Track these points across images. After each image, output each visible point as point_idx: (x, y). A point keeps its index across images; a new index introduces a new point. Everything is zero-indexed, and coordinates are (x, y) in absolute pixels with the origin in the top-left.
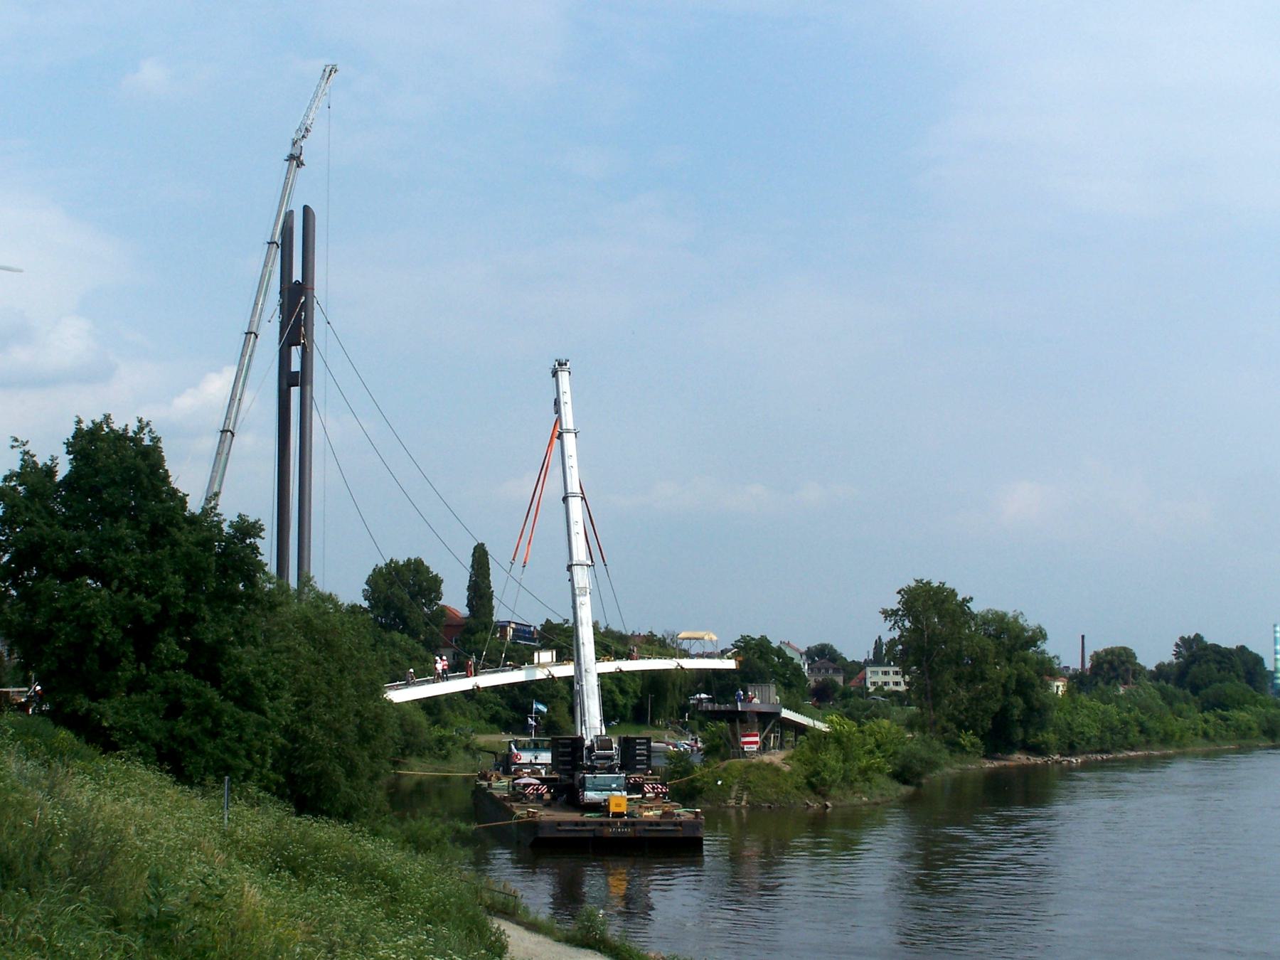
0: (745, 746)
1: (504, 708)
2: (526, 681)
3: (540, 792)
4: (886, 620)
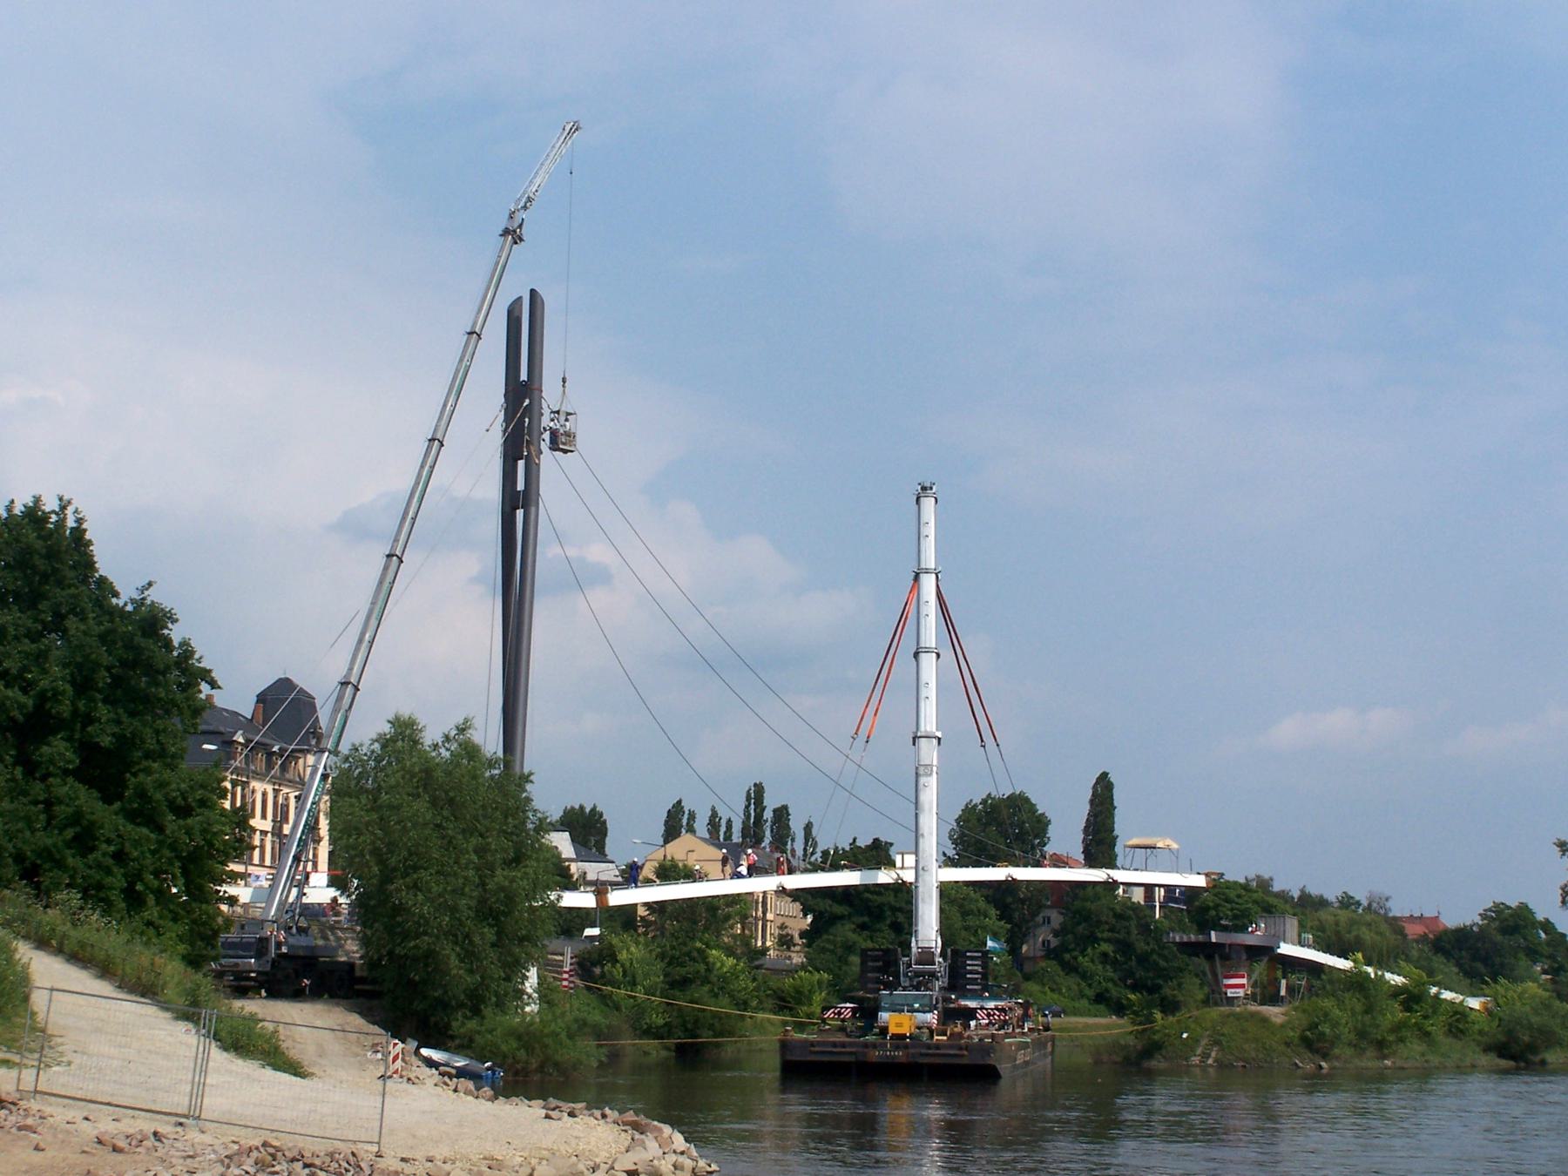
0: (1229, 991)
1: (1115, 984)
2: (860, 885)
3: (842, 1016)
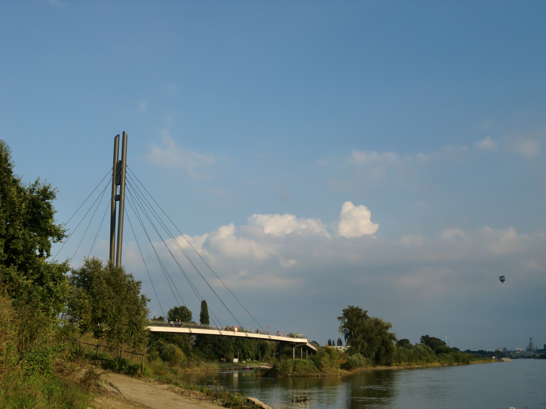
4: (339, 320)
